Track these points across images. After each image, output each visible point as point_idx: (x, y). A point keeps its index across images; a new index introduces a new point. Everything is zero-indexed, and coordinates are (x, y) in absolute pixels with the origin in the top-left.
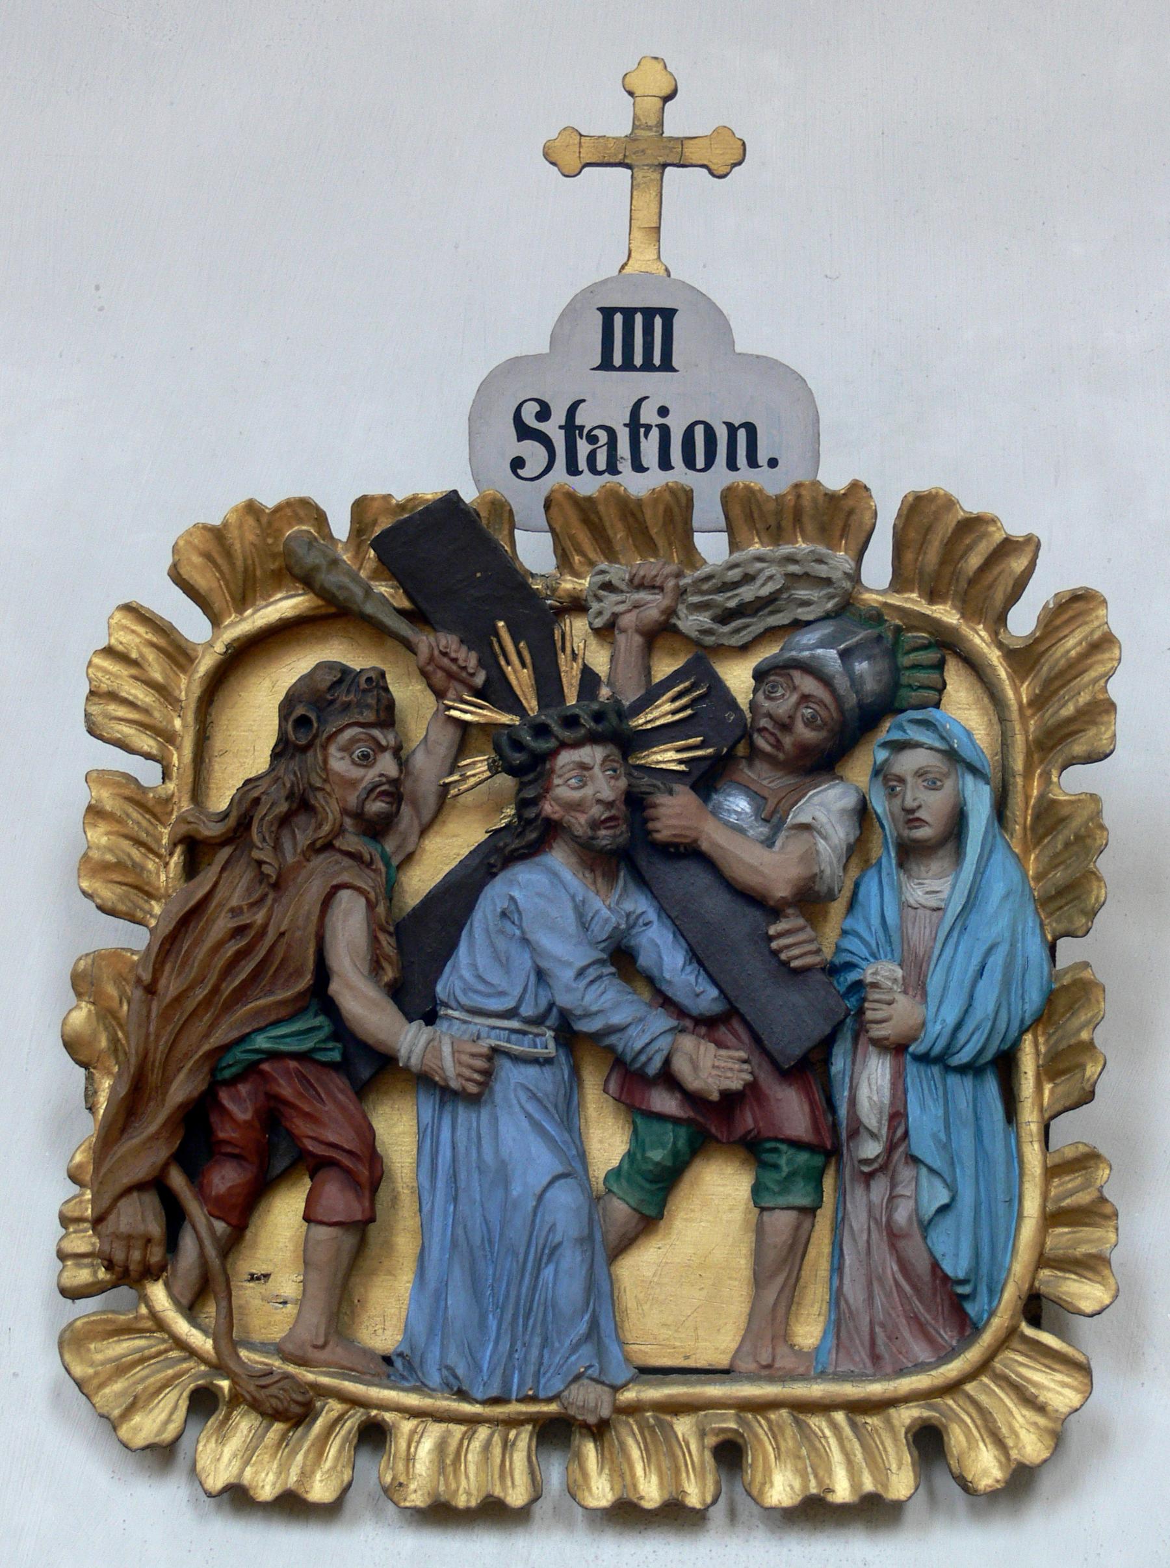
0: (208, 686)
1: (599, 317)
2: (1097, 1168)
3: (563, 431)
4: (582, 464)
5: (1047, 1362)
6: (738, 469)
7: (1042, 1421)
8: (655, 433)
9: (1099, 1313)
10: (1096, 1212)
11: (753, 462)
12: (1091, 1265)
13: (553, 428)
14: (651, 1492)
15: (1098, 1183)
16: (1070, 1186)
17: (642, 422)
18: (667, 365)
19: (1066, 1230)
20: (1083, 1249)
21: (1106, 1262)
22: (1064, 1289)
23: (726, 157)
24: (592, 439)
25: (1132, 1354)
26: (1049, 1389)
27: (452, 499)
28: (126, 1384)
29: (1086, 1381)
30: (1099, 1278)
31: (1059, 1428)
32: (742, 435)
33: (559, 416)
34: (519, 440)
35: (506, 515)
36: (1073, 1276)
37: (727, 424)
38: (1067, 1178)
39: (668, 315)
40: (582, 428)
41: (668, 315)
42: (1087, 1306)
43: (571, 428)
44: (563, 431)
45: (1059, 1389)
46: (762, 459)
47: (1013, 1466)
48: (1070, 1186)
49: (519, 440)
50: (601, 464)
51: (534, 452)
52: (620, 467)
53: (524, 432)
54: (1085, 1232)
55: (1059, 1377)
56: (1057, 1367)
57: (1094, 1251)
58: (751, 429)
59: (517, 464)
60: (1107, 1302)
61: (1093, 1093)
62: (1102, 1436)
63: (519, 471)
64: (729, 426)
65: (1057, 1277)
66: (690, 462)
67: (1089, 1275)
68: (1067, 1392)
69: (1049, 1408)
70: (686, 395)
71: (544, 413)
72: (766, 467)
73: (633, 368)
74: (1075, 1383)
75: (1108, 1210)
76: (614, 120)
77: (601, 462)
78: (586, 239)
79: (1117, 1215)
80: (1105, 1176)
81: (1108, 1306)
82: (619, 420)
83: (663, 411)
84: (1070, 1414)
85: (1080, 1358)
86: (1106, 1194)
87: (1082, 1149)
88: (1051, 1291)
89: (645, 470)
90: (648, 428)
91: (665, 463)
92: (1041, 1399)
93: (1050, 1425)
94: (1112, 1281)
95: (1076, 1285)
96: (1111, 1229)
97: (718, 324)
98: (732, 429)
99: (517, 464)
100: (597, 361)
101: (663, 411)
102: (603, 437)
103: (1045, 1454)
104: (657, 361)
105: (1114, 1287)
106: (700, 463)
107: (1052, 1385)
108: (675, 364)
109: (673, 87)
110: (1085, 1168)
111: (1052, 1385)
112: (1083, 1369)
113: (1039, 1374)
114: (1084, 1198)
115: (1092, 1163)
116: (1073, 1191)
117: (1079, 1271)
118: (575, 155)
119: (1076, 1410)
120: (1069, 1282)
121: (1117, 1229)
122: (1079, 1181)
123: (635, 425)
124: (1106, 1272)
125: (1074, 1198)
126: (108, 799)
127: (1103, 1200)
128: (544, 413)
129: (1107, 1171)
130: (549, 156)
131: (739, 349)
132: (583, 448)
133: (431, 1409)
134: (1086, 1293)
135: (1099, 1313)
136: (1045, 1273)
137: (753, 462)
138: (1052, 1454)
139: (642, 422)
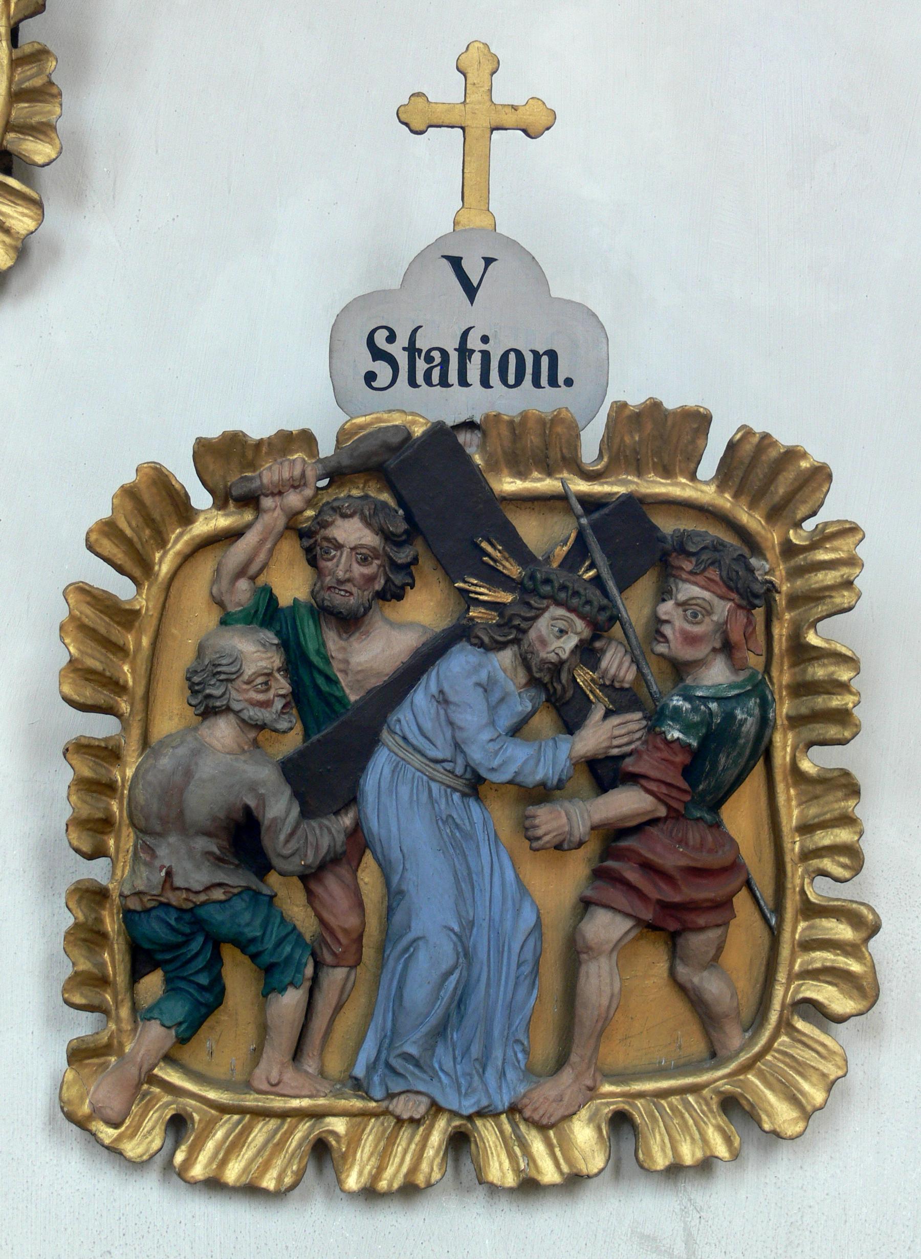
2: (48, 60)
3: (407, 353)
4: (420, 379)
5: (12, 198)
7: (7, 240)
8: (477, 358)
9: (48, 164)
10: (45, 93)
11: (553, 382)
12: (42, 130)
15: (48, 72)
16: (29, 73)
17: (417, 346)
19: (26, 105)
20: (35, 120)
21: (54, 128)
22: (24, 147)
24: (429, 359)
25: (77, 195)
26: (12, 218)
28: (243, 1164)
29: (39, 212)
30: (48, 140)
31: (19, 244)
32: (545, 361)
33: (403, 340)
34: (374, 360)
36: (31, 138)
38: (27, 68)
40: (420, 351)
42: (39, 159)
43: (412, 350)
44: (407, 353)
45: (20, 218)
46: (561, 381)
48: (29, 73)
49: (374, 360)
51: (383, 371)
52: (450, 381)
53: (378, 354)
54: (39, 106)
55: (20, 209)
56: (19, 202)
57: (44, 120)
58: (553, 355)
59: (370, 377)
60: (54, 156)
61: (44, 6)
62: (55, 252)
63: (374, 384)
64: (536, 354)
65: (20, 138)
67: (41, 137)
68: (26, 219)
69: (13, 231)
71: (391, 338)
74: (31, 214)
75: (54, 91)
78: (425, 192)
79: (61, 95)
80: (53, 67)
81: (54, 160)
82: (451, 346)
84: (28, 235)
85: (34, 195)
86: (54, 79)
87: (36, 46)
88: (15, 148)
91: (485, 382)
92: (7, 224)
93: (14, 243)
94: (57, 141)
95: (33, 144)
96: (57, 105)
98: (537, 356)
99: (370, 377)
101: (485, 339)
102: (436, 355)
103: (10, 263)
105: (58, 146)
107: (15, 215)
110: (40, 61)
111: (15, 215)
112: (37, 204)
113: (6, 207)
114: (38, 82)
115: (44, 57)
116: (30, 77)
117: (35, 134)
118: (417, 118)
119: (32, 233)
120: (28, 143)
121: (61, 105)
122: (34, 70)
123: (464, 352)
124: (53, 135)
125: (31, 82)
127: (51, 83)
128: (391, 338)
129: (54, 63)
132: (421, 366)
134: (38, 150)
135: (48, 164)
136: (11, 136)
137: (553, 382)
138: (15, 263)
139: (417, 346)
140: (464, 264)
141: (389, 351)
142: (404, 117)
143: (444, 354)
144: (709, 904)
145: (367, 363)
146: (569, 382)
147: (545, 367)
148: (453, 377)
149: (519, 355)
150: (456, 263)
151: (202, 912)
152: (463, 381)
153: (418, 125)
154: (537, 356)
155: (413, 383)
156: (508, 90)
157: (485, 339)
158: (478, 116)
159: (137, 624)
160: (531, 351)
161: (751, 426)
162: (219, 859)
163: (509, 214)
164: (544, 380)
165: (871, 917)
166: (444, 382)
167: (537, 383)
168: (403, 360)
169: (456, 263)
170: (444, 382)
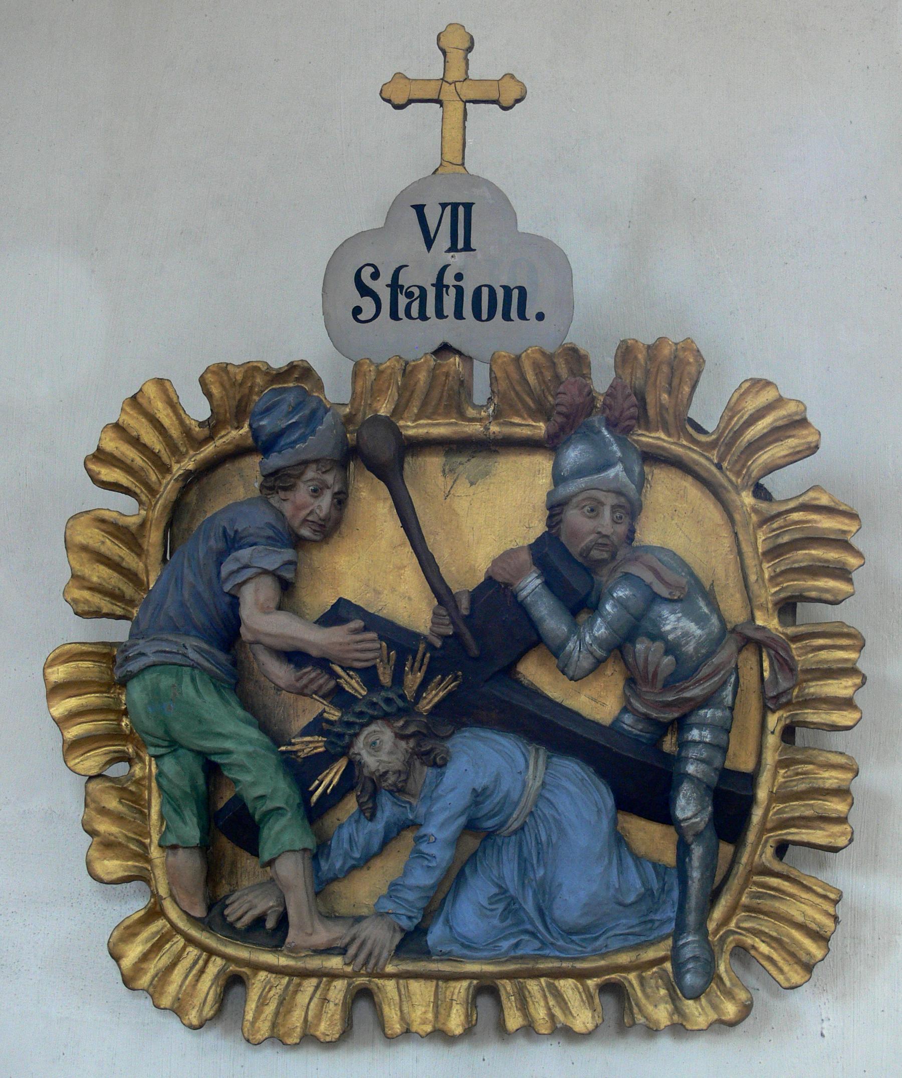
0: (81, 709)
1: (413, 212)
3: (389, 289)
4: (401, 313)
6: (463, 318)
8: (452, 291)
11: (522, 316)
13: (381, 287)
17: (445, 283)
18: (468, 247)
23: (505, 97)
24: (409, 295)
27: (300, 372)
32: (515, 294)
37: (504, 287)
39: (468, 207)
40: (402, 287)
41: (468, 207)
43: (395, 286)
44: (389, 289)
46: (531, 312)
50: (415, 312)
51: (368, 305)
52: (428, 315)
53: (364, 290)
58: (522, 291)
59: (357, 311)
63: (360, 317)
66: (477, 315)
70: (478, 270)
71: (375, 276)
72: (533, 320)
77: (415, 307)
78: (405, 151)
82: (428, 281)
83: (459, 277)
90: (447, 287)
91: (459, 315)
97: (504, 207)
98: (508, 291)
99: (357, 311)
101: (459, 277)
102: (417, 292)
106: (485, 316)
108: (472, 246)
109: (468, 38)
123: (440, 285)
126: (93, 537)
128: (375, 276)
132: (403, 301)
133: (763, 761)
139: (445, 283)
140: (426, 210)
142: (443, 43)
144: (172, 395)
145: (356, 299)
147: (511, 303)
148: (430, 310)
150: (419, 209)
151: (199, 912)
152: (440, 314)
154: (508, 291)
155: (394, 315)
156: (484, 66)
158: (454, 86)
159: (326, 851)
161: (764, 377)
164: (514, 314)
165: (428, 655)
166: (423, 317)
168: (385, 296)
169: (419, 209)
170: (423, 317)
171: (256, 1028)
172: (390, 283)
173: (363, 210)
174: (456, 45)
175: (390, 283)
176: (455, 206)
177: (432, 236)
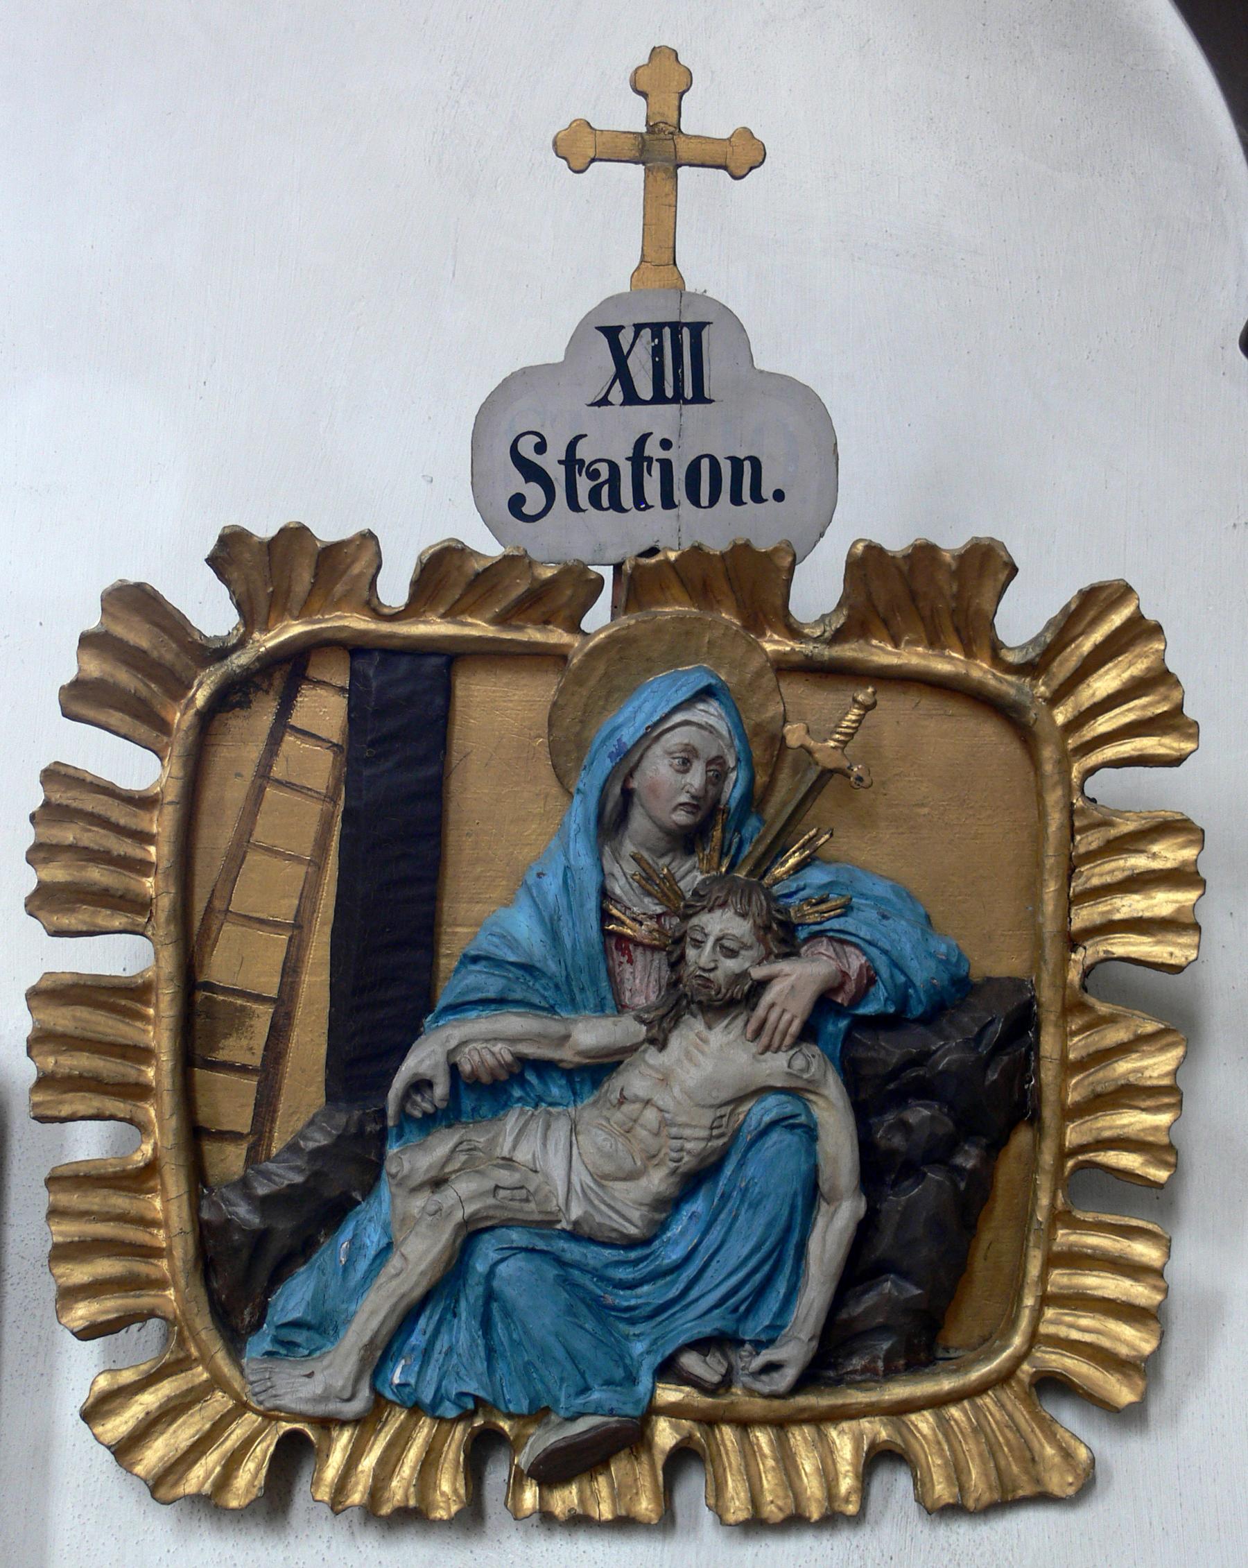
1: (603, 342)
3: (563, 467)
8: (656, 467)
11: (757, 497)
14: (774, 1505)
17: (646, 454)
18: (700, 397)
24: (594, 475)
32: (747, 466)
33: (556, 450)
34: (527, 482)
35: (624, 580)
39: (697, 329)
40: (582, 462)
41: (697, 329)
43: (571, 462)
44: (563, 467)
46: (767, 492)
47: (154, 1062)
49: (527, 482)
51: (535, 496)
53: (531, 472)
58: (756, 463)
59: (516, 503)
70: (694, 433)
71: (541, 448)
73: (665, 401)
76: (702, 117)
78: (577, 254)
82: (621, 453)
89: (648, 507)
90: (650, 460)
91: (668, 502)
98: (736, 463)
99: (516, 503)
100: (705, 333)
101: (666, 444)
102: (604, 470)
104: (669, 393)
118: (580, 148)
123: (639, 459)
128: (541, 448)
130: (559, 148)
131: (559, 357)
132: (584, 485)
139: (646, 454)
141: (538, 463)
142: (562, 151)
143: (614, 468)
145: (517, 482)
146: (779, 496)
148: (627, 497)
149: (694, 499)
152: (640, 501)
153: (739, 173)
154: (736, 463)
155: (574, 505)
157: (666, 444)
160: (728, 458)
162: (712, 1461)
163: (706, 269)
166: (616, 505)
167: (737, 499)
168: (558, 474)
170: (616, 505)
171: (357, 1245)
172: (563, 458)
173: (543, 330)
174: (663, 76)
175: (563, 458)
176: (657, 329)
177: (618, 383)
